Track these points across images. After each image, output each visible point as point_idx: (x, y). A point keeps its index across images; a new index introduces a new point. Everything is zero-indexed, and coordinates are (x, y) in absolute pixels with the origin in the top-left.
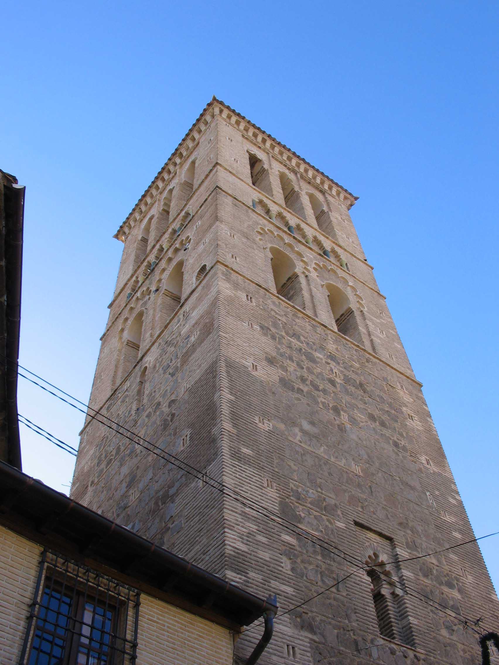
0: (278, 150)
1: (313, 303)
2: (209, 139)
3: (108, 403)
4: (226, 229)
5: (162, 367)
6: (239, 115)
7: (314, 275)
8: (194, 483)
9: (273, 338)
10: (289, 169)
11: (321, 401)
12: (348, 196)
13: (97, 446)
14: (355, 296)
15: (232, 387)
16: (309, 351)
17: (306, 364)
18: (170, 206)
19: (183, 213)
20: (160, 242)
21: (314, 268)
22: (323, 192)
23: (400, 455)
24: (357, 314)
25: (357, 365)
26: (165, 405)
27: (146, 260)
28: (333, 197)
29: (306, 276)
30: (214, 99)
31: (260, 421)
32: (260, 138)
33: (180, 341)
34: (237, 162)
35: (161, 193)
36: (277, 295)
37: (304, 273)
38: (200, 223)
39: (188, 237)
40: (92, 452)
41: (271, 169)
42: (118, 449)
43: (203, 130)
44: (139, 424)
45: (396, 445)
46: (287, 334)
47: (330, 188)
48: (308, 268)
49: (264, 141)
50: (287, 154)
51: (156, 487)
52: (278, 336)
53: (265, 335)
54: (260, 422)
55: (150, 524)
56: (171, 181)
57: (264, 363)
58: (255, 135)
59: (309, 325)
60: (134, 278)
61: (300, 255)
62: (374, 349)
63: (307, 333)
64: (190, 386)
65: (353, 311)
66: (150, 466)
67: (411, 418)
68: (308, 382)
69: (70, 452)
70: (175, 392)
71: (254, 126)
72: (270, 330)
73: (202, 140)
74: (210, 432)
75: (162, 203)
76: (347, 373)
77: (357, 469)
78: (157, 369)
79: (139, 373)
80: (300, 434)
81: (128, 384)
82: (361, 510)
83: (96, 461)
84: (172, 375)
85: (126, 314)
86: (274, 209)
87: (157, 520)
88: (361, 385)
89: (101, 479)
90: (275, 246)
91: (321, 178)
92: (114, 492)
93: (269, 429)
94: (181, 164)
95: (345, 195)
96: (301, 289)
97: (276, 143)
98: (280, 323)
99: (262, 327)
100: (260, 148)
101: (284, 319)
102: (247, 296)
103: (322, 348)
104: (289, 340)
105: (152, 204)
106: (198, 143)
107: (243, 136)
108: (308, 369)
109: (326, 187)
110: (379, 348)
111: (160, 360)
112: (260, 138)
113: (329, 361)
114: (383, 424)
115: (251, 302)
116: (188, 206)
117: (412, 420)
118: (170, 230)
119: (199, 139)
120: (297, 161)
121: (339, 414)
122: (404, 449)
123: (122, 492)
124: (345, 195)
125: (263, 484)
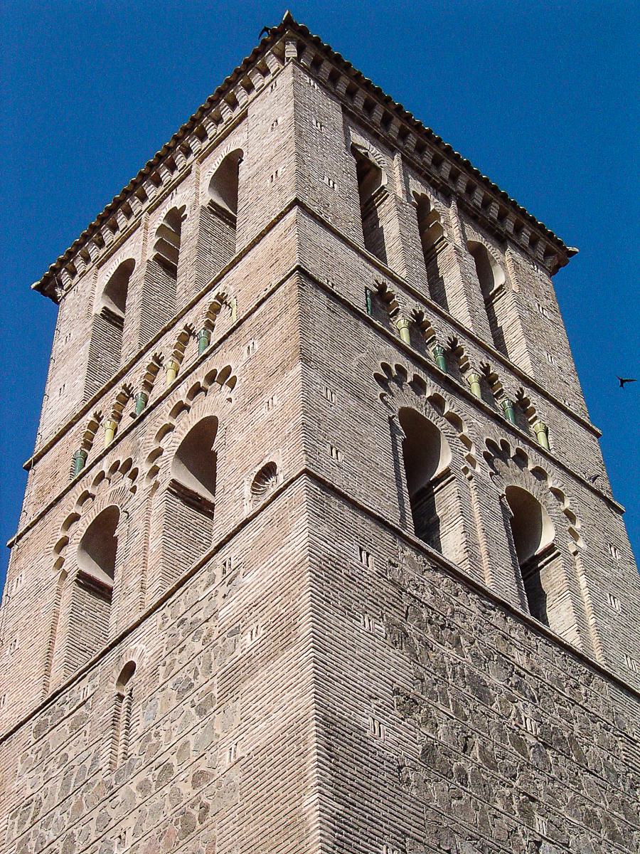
0: (415, 141)
2: (273, 119)
3: (39, 718)
5: (174, 680)
6: (338, 59)
12: (555, 248)
13: (14, 816)
15: (338, 781)
18: (178, 253)
19: (211, 297)
26: (183, 776)
27: (121, 383)
30: (289, 22)
32: (378, 114)
33: (216, 635)
35: (151, 211)
38: (256, 347)
43: (257, 87)
44: (119, 799)
47: (518, 229)
49: (386, 121)
50: (432, 150)
56: (175, 187)
58: (369, 107)
61: (455, 421)
64: (244, 754)
70: (208, 755)
71: (368, 85)
78: (161, 681)
81: (86, 687)
82: (433, 671)
84: (201, 711)
85: (70, 504)
94: (203, 157)
95: (547, 246)
97: (411, 125)
100: (376, 136)
109: (509, 226)
111: (168, 660)
112: (378, 114)
119: (248, 104)
120: (453, 168)
124: (547, 246)
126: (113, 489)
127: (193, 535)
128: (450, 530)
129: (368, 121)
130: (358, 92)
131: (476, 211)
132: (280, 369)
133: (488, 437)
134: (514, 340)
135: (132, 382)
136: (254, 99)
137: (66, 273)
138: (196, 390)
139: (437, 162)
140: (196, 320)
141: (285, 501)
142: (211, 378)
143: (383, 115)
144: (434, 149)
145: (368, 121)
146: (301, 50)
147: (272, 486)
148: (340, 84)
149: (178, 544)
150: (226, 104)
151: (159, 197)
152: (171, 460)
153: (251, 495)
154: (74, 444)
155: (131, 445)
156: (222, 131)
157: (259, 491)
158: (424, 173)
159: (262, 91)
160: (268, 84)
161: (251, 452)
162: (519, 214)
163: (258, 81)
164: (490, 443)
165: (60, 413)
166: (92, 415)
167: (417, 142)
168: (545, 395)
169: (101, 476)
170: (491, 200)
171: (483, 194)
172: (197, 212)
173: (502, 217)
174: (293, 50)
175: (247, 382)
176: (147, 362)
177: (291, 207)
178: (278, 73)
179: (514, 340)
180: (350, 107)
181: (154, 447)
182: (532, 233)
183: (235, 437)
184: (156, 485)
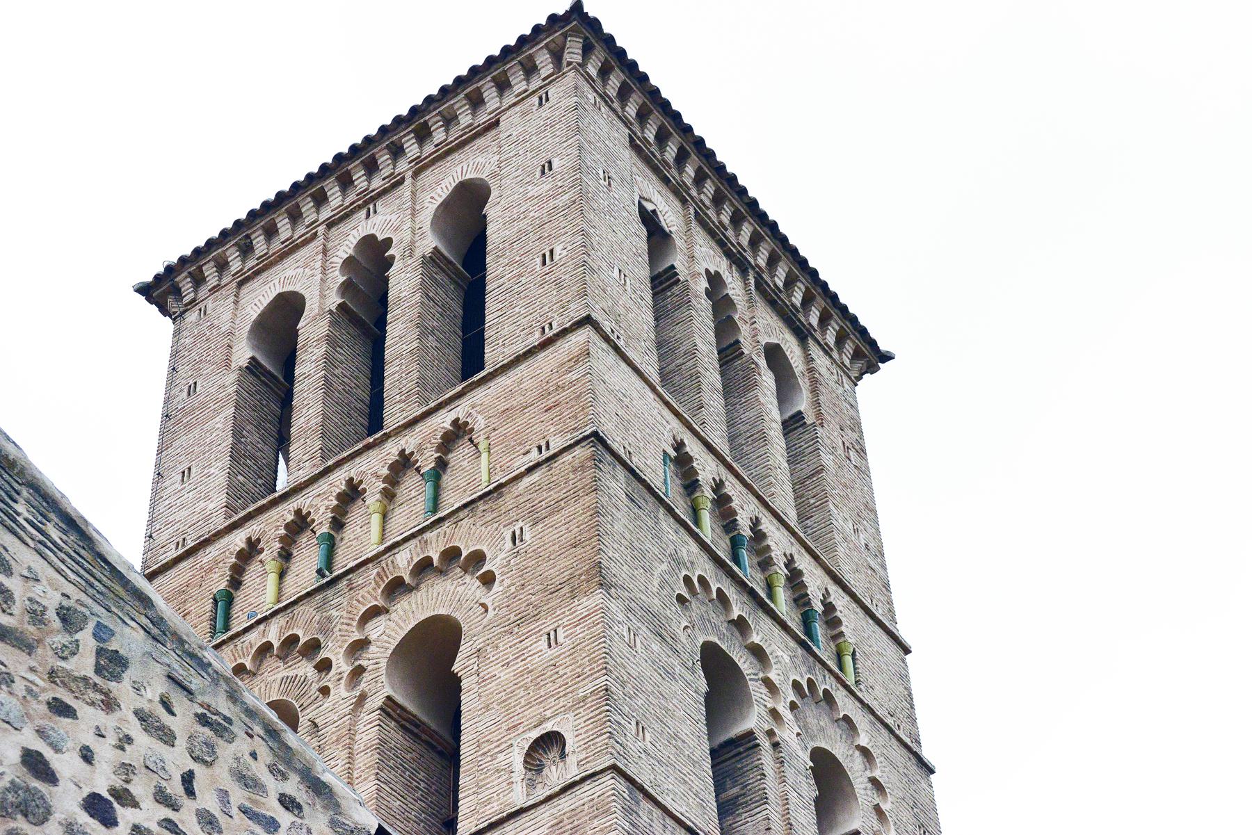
14: (869, 785)
22: (802, 334)
28: (827, 351)
37: (770, 733)
50: (732, 204)
73: (512, 124)
91: (807, 288)
95: (857, 346)
100: (665, 180)
105: (292, 248)
124: (857, 346)
126: (285, 674)
127: (410, 776)
128: (749, 819)
129: (658, 160)
130: (651, 117)
131: (776, 294)
132: (566, 589)
133: (720, 586)
134: (812, 501)
135: (312, 511)
136: (510, 107)
137: (189, 280)
138: (424, 567)
139: (737, 221)
140: (420, 449)
141: (582, 802)
142: (451, 555)
143: (678, 150)
144: (736, 203)
145: (658, 160)
146: (587, 50)
147: (556, 774)
148: (593, 57)
149: (394, 793)
150: (465, 102)
151: (347, 207)
152: (384, 663)
153: (524, 771)
154: (215, 576)
155: (317, 618)
156: (456, 139)
157: (532, 764)
158: (718, 238)
159: (523, 99)
160: (534, 92)
161: (523, 703)
162: (829, 301)
163: (519, 84)
164: (796, 685)
165: (184, 513)
166: (244, 540)
167: (715, 191)
168: (853, 596)
169: (266, 648)
170: (798, 280)
171: (787, 270)
172: (415, 262)
173: (790, 283)
174: (577, 51)
175: (513, 589)
176: (337, 486)
177: (579, 324)
178: (549, 80)
179: (812, 501)
180: (638, 138)
181: (357, 636)
182: (841, 327)
183: (496, 670)
184: (362, 698)
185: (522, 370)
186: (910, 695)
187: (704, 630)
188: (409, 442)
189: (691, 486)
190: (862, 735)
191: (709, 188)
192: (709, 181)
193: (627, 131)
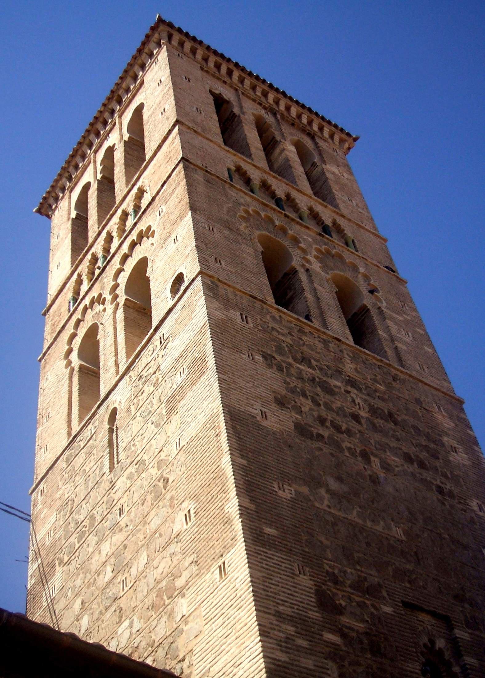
1: (320, 307)
4: (203, 221)
7: (316, 266)
8: (209, 574)
9: (280, 369)
10: (265, 108)
11: (346, 447)
16: (325, 379)
17: (323, 398)
20: (108, 228)
21: (316, 257)
22: (312, 136)
23: (446, 503)
24: (374, 312)
25: (382, 388)
29: (307, 270)
31: (279, 487)
34: (201, 113)
35: (96, 152)
36: (277, 306)
37: (303, 266)
39: (149, 228)
40: (53, 519)
41: (244, 113)
42: (93, 518)
45: (440, 490)
46: (295, 360)
48: (308, 257)
50: (260, 87)
51: (156, 574)
52: (284, 365)
53: (270, 366)
54: (280, 489)
55: (154, 623)
56: (108, 135)
57: (274, 407)
59: (320, 341)
60: (75, 276)
62: (400, 360)
63: (319, 353)
65: (369, 309)
66: (142, 546)
67: (455, 450)
68: (328, 424)
69: (22, 512)
72: (275, 359)
73: (145, 79)
74: (222, 508)
75: (99, 168)
76: (372, 401)
77: (398, 532)
79: (107, 417)
80: (327, 496)
83: (61, 533)
86: (255, 176)
87: (165, 619)
88: (390, 415)
89: (73, 557)
90: (264, 232)
91: (308, 116)
92: (96, 576)
93: (291, 497)
96: (303, 290)
98: (284, 345)
99: (265, 356)
101: (288, 340)
102: (241, 315)
103: (339, 372)
104: (298, 368)
106: (142, 83)
107: (202, 69)
108: (326, 404)
110: (409, 360)
113: (349, 388)
114: (422, 465)
115: (247, 323)
116: (141, 179)
117: (456, 453)
118: (119, 212)
119: (143, 76)
121: (369, 461)
122: (451, 494)
123: (107, 579)
125: (294, 571)
185: (159, 154)
186: (389, 256)
187: (258, 229)
188: (123, 207)
189: (248, 181)
190: (361, 269)
191: (247, 82)
192: (246, 80)
193: (199, 65)
